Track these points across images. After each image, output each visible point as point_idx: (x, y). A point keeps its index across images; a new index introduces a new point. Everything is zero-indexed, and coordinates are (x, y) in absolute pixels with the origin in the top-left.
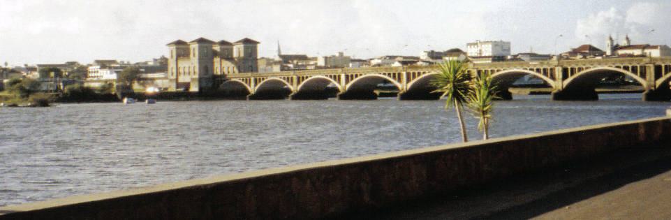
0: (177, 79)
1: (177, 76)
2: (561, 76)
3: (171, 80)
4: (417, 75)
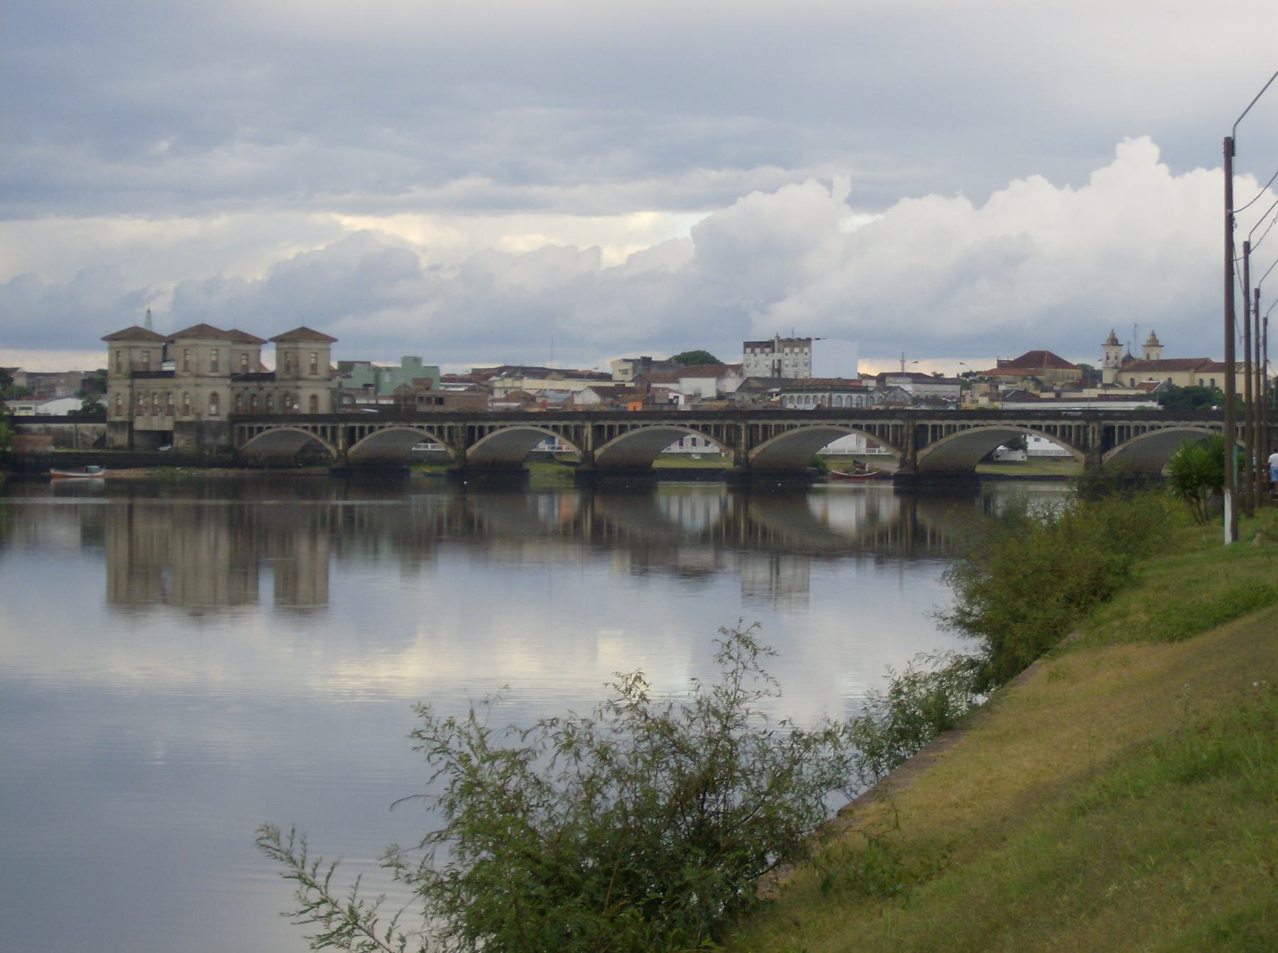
0: (131, 424)
1: (130, 415)
2: (1098, 443)
3: (114, 425)
4: (255, 431)
